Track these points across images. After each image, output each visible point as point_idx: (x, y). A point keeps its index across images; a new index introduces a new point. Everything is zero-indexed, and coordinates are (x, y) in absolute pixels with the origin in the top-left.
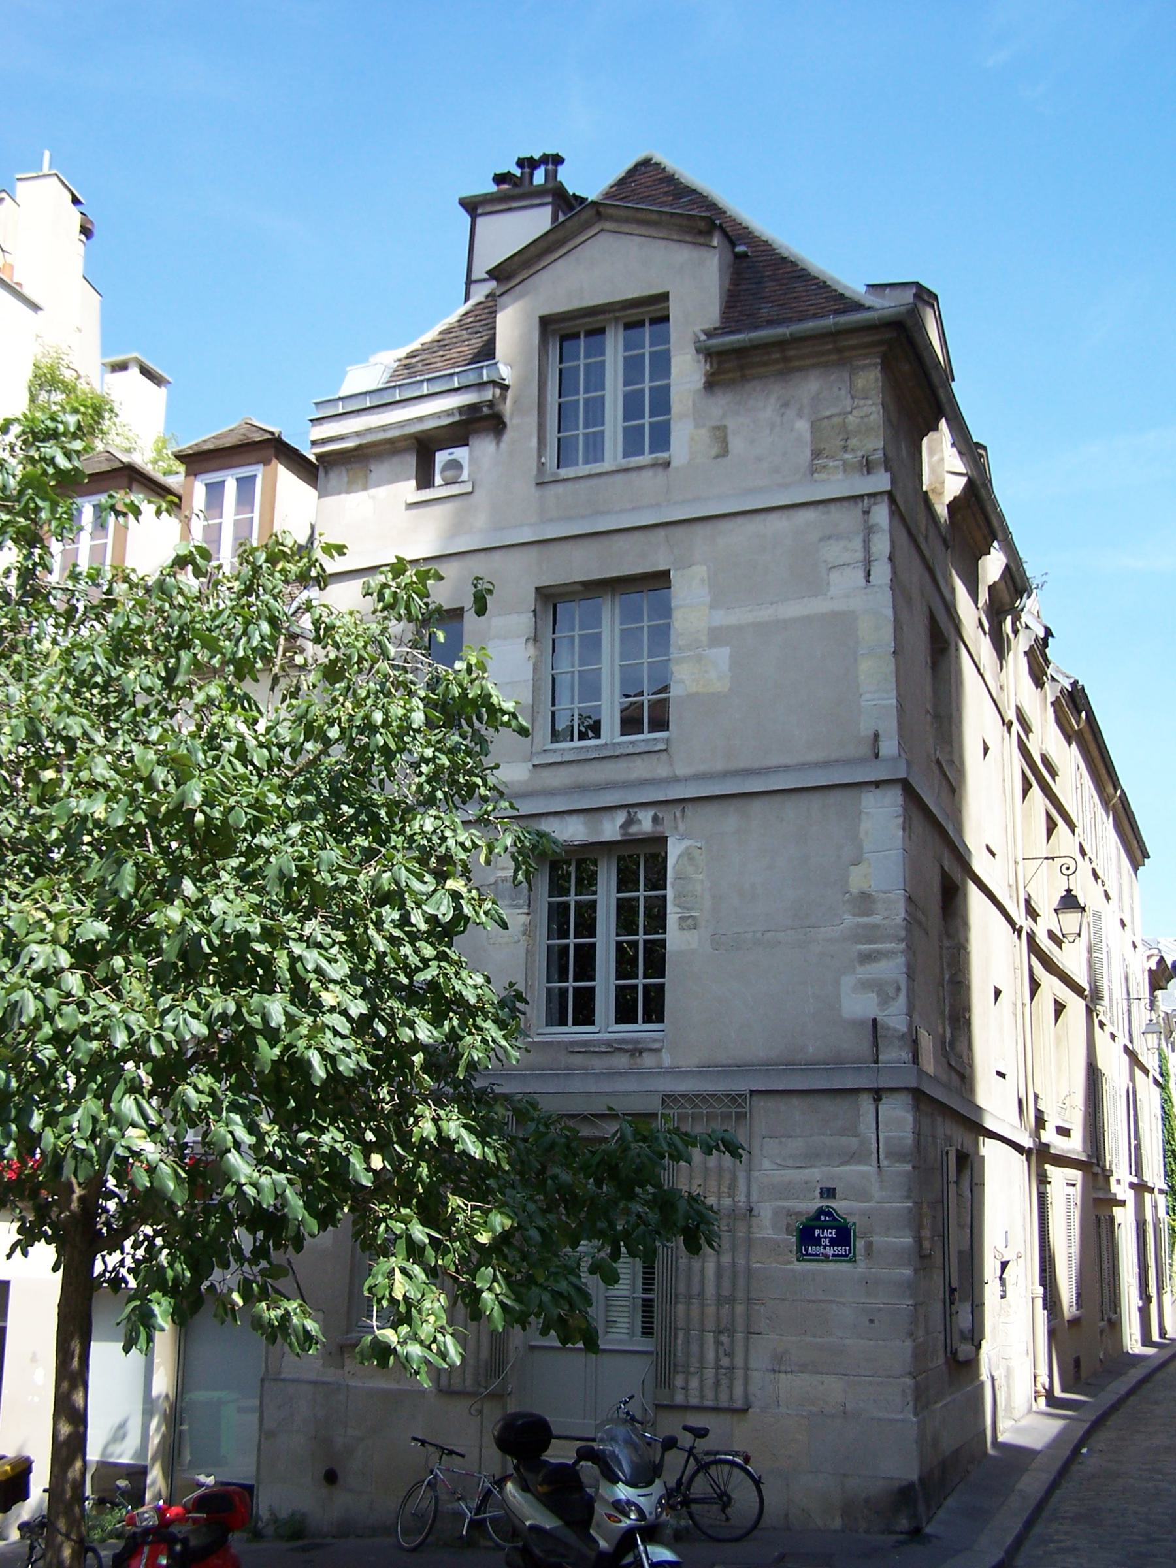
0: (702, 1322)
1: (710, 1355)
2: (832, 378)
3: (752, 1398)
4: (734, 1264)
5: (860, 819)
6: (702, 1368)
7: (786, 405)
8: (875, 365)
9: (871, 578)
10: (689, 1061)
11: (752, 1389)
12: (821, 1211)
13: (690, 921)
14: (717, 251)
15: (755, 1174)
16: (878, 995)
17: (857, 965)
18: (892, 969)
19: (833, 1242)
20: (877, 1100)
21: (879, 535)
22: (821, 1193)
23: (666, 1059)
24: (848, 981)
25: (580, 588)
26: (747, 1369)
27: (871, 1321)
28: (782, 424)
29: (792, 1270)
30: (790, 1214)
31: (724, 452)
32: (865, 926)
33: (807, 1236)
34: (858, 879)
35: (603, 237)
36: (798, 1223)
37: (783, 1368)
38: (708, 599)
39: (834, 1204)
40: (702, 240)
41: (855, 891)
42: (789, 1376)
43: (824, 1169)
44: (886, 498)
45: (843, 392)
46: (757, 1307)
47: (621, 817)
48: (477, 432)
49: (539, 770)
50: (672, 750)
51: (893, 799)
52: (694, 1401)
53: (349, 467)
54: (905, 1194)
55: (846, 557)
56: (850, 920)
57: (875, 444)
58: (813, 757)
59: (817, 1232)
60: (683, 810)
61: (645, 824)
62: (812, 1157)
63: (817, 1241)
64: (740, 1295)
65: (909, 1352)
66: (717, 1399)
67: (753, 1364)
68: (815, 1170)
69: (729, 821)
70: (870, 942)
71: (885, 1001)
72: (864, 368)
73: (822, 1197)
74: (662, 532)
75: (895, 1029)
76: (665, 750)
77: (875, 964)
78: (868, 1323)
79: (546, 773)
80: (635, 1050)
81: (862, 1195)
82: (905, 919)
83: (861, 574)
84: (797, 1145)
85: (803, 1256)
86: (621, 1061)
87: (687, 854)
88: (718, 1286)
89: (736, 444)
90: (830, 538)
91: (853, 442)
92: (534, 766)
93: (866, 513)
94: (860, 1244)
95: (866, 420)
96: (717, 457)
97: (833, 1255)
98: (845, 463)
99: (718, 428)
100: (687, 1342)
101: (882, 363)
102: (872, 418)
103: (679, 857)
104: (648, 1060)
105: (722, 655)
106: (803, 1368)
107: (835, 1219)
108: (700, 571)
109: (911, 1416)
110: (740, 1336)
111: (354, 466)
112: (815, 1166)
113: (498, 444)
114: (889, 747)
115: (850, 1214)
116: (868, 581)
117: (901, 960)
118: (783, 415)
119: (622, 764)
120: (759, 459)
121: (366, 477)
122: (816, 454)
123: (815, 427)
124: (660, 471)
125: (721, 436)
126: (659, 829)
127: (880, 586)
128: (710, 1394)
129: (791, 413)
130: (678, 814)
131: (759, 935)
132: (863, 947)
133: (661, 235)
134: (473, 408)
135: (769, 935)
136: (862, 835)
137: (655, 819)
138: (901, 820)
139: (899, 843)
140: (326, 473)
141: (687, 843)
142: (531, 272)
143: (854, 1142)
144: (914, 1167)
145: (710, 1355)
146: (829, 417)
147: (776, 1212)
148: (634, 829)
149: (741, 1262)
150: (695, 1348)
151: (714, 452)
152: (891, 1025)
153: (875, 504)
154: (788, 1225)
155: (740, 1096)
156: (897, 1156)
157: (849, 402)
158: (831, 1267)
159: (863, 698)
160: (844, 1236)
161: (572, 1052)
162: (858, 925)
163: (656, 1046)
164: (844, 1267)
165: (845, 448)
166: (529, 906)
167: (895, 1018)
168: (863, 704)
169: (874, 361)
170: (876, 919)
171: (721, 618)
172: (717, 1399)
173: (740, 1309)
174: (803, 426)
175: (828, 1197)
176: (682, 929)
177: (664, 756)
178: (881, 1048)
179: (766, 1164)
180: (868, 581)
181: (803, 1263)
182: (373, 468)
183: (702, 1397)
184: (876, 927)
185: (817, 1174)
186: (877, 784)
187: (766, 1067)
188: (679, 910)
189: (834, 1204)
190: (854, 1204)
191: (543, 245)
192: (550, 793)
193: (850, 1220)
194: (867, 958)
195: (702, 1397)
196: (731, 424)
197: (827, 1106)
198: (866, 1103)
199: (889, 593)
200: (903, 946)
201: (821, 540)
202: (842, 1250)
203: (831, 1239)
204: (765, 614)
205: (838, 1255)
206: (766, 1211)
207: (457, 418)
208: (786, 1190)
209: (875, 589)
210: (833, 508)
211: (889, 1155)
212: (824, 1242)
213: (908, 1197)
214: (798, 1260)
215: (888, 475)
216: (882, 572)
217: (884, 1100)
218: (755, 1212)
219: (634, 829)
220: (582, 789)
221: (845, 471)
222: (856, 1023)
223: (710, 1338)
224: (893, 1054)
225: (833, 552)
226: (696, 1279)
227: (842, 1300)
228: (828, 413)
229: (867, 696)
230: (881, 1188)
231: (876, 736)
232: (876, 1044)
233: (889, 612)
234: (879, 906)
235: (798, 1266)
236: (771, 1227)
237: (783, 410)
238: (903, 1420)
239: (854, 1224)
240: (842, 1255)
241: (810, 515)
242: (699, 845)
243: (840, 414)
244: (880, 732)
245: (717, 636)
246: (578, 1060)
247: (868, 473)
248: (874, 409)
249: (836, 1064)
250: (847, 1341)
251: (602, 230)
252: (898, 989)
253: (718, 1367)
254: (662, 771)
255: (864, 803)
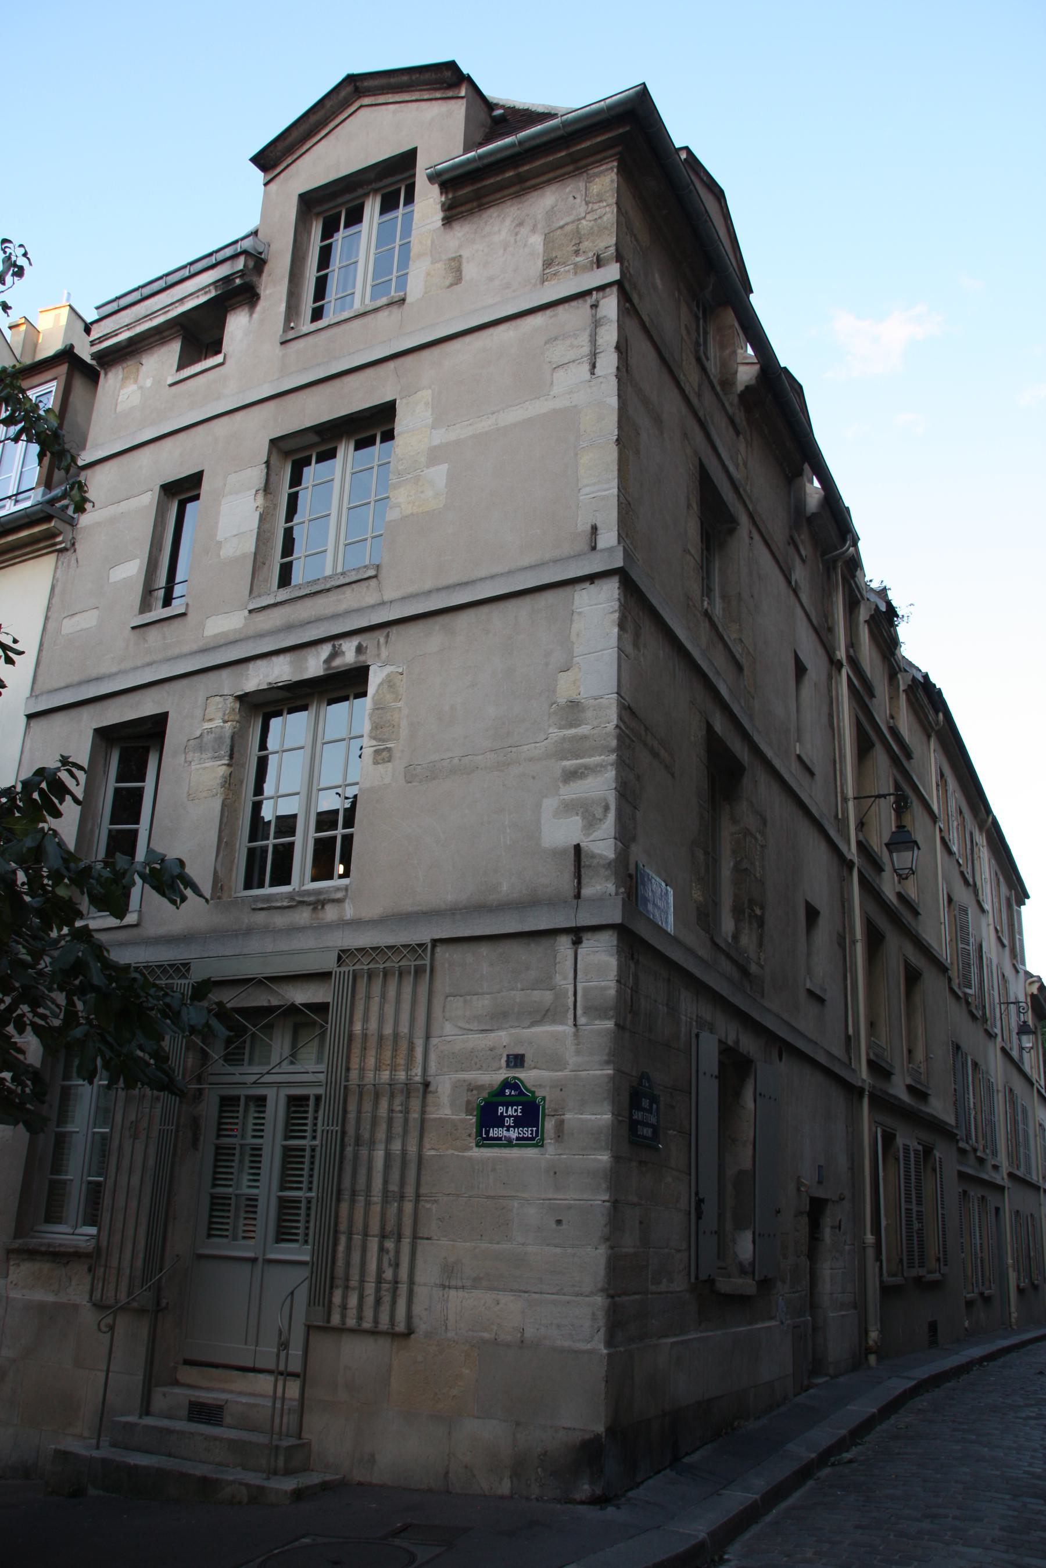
0: (366, 1226)
1: (372, 1266)
2: (567, 190)
3: (416, 1321)
4: (404, 1152)
5: (571, 621)
6: (362, 1281)
7: (521, 224)
8: (612, 169)
9: (596, 370)
10: (373, 911)
11: (418, 1309)
12: (506, 1084)
13: (385, 754)
14: (465, 100)
15: (434, 1041)
16: (584, 818)
17: (561, 785)
18: (601, 785)
19: (519, 1123)
20: (577, 942)
21: (607, 327)
22: (508, 1062)
23: (349, 911)
24: (550, 804)
25: (314, 438)
26: (411, 1282)
27: (559, 1222)
28: (516, 242)
29: (470, 1159)
30: (471, 1088)
31: (458, 279)
32: (574, 739)
33: (488, 1116)
34: (566, 688)
35: (363, 112)
36: (479, 1098)
37: (453, 1283)
38: (430, 421)
39: (522, 1074)
40: (450, 94)
41: (562, 701)
42: (461, 1293)
43: (513, 1031)
44: (615, 289)
45: (578, 200)
46: (428, 1206)
47: (326, 650)
48: (234, 308)
49: (254, 615)
50: (381, 577)
51: (609, 591)
52: (351, 1322)
53: (125, 365)
54: (605, 1058)
55: (571, 355)
56: (556, 734)
57: (608, 242)
58: (526, 561)
59: (501, 1109)
60: (388, 636)
61: (349, 654)
62: (499, 1017)
63: (499, 1122)
64: (410, 1190)
65: (603, 1261)
66: (376, 1321)
67: (419, 1278)
68: (502, 1033)
69: (430, 639)
70: (577, 756)
71: (591, 823)
72: (598, 175)
73: (508, 1066)
74: (391, 365)
75: (601, 856)
76: (375, 576)
77: (580, 782)
78: (554, 1226)
79: (260, 617)
80: (317, 902)
81: (556, 1062)
82: (617, 726)
83: (586, 367)
84: (482, 1004)
85: (484, 1140)
86: (304, 916)
87: (389, 683)
88: (386, 1182)
89: (470, 271)
90: (556, 339)
91: (586, 245)
92: (250, 611)
93: (595, 306)
94: (549, 1125)
95: (599, 221)
96: (452, 285)
97: (518, 1139)
98: (576, 264)
99: (453, 259)
100: (349, 1249)
101: (618, 167)
102: (605, 218)
103: (381, 684)
104: (330, 913)
105: (439, 474)
106: (476, 1283)
107: (521, 1093)
108: (426, 395)
109: (602, 1346)
110: (406, 1242)
111: (129, 363)
112: (502, 1029)
113: (251, 315)
114: (609, 538)
115: (540, 1086)
116: (593, 374)
117: (611, 774)
118: (516, 234)
119: (332, 597)
120: (491, 279)
121: (138, 370)
122: (548, 263)
123: (548, 240)
124: (395, 309)
125: (456, 269)
126: (362, 658)
127: (605, 377)
128: (368, 1313)
129: (524, 231)
130: (382, 640)
131: (456, 761)
132: (567, 763)
133: (414, 98)
134: (227, 279)
135: (466, 760)
136: (573, 638)
137: (360, 649)
138: (616, 615)
139: (614, 641)
140: (106, 374)
141: (389, 669)
142: (295, 156)
143: (548, 996)
144: (616, 1024)
145: (372, 1266)
146: (562, 227)
147: (455, 1087)
148: (337, 662)
149: (412, 1149)
150: (356, 1257)
151: (447, 283)
152: (597, 851)
153: (603, 298)
154: (468, 1102)
155: (420, 945)
156: (596, 1011)
157: (582, 209)
158: (515, 1153)
159: (584, 491)
160: (531, 1113)
161: (254, 909)
162: (564, 739)
163: (339, 895)
164: (531, 1153)
165: (577, 253)
166: (231, 757)
167: (602, 844)
168: (581, 498)
169: (609, 166)
170: (584, 730)
171: (439, 437)
172: (376, 1321)
173: (408, 1207)
174: (537, 241)
175: (516, 1066)
176: (376, 763)
177: (373, 583)
178: (584, 881)
179: (449, 1028)
180: (593, 374)
181: (483, 1150)
182: (144, 361)
183: (360, 1318)
184: (584, 738)
185: (504, 1038)
186: (591, 578)
187: (453, 912)
188: (374, 743)
189: (522, 1074)
190: (545, 1074)
191: (303, 128)
192: (261, 636)
193: (540, 1093)
194: (572, 775)
195: (360, 1318)
196: (465, 253)
197: (518, 952)
198: (564, 943)
199: (614, 382)
200: (613, 757)
201: (546, 343)
202: (527, 1132)
203: (516, 1117)
204: (485, 425)
205: (523, 1139)
206: (444, 1086)
207: (213, 294)
208: (467, 1060)
209: (601, 379)
210: (560, 309)
211: (587, 1010)
212: (509, 1122)
213: (608, 1062)
214: (478, 1146)
215: (618, 265)
216: (608, 362)
217: (585, 943)
218: (431, 1088)
219: (337, 662)
220: (289, 628)
221: (576, 273)
222: (557, 853)
223: (373, 1244)
224: (601, 886)
225: (559, 352)
226: (363, 1171)
227: (524, 1195)
228: (562, 223)
229: (587, 490)
230: (578, 1052)
231: (594, 529)
232: (578, 875)
233: (614, 401)
234: (589, 714)
235: (478, 1153)
236: (448, 1106)
237: (518, 229)
238: (590, 1352)
239: (544, 1099)
240: (527, 1139)
241: (537, 320)
242: (400, 670)
243: (573, 222)
244: (598, 525)
245: (435, 455)
246: (261, 918)
247: (598, 267)
248: (607, 209)
249: (531, 903)
250: (530, 1249)
251: (361, 106)
252: (607, 808)
253: (379, 1280)
254: (371, 599)
255: (577, 603)
